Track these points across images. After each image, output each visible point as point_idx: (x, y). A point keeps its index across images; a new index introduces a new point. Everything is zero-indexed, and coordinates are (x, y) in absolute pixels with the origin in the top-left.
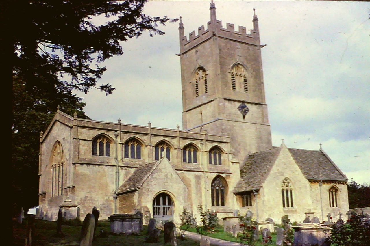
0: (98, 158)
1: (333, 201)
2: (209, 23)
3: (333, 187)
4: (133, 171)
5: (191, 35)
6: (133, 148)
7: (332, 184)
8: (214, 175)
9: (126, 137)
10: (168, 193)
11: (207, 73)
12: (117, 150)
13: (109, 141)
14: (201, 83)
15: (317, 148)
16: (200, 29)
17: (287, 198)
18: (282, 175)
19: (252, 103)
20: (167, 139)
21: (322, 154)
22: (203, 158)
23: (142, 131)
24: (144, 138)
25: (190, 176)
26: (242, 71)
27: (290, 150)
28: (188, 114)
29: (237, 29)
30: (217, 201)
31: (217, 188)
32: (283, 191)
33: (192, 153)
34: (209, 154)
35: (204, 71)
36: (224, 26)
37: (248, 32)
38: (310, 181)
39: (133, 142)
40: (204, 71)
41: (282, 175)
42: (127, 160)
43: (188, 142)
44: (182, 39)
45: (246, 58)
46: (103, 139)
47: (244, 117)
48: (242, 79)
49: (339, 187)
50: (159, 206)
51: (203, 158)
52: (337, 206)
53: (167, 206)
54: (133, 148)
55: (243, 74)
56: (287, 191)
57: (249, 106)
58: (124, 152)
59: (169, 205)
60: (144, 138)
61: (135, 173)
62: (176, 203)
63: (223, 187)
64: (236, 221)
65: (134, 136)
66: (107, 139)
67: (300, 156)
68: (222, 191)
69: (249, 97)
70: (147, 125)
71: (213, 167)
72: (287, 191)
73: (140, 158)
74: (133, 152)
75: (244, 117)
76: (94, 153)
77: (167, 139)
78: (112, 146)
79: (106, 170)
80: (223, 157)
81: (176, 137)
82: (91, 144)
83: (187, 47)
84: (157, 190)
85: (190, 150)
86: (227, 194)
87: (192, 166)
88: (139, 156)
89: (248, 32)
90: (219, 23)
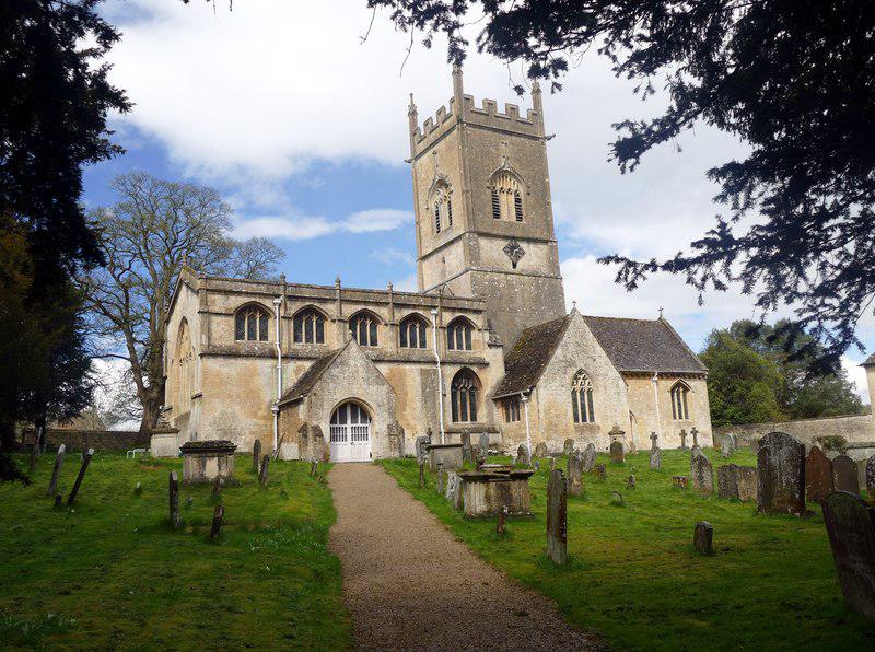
0: (244, 344)
1: (680, 411)
2: (452, 101)
3: (678, 385)
4: (308, 365)
5: (426, 124)
9: (294, 308)
11: (452, 188)
12: (278, 333)
13: (266, 314)
14: (444, 208)
15: (655, 318)
16: (439, 113)
17: (583, 410)
18: (572, 364)
22: (435, 341)
23: (381, 299)
25: (413, 373)
26: (509, 184)
27: (588, 319)
29: (501, 110)
30: (462, 414)
32: (574, 392)
33: (463, 333)
34: (295, 324)
35: (447, 186)
36: (478, 105)
37: (523, 115)
38: (625, 375)
40: (447, 186)
42: (297, 346)
43: (407, 312)
44: (414, 131)
45: (518, 160)
47: (514, 266)
51: (435, 341)
52: (687, 417)
53: (338, 425)
54: (459, 336)
55: (514, 188)
56: (582, 392)
58: (292, 331)
61: (313, 367)
62: (375, 418)
63: (473, 388)
64: (453, 456)
65: (308, 303)
68: (472, 395)
69: (529, 225)
70: (333, 284)
72: (582, 392)
75: (514, 266)
78: (270, 321)
80: (475, 335)
81: (388, 304)
82: (232, 321)
84: (340, 396)
85: (412, 326)
87: (417, 352)
88: (321, 339)
89: (523, 115)
90: (469, 99)
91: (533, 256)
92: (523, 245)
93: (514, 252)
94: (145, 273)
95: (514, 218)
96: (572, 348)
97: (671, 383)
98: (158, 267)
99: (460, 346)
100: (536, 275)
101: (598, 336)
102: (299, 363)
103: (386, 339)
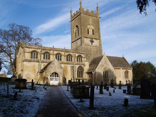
6: (79, 59)
7: (126, 70)
8: (79, 66)
10: (57, 72)
15: (122, 57)
19: (95, 39)
20: (60, 52)
21: (123, 58)
23: (51, 49)
24: (51, 52)
27: (107, 56)
28: (73, 43)
31: (80, 71)
39: (47, 54)
41: (104, 66)
46: (35, 52)
47: (92, 44)
48: (92, 30)
49: (129, 71)
50: (53, 77)
52: (128, 78)
54: (79, 59)
57: (94, 40)
59: (57, 77)
60: (51, 52)
66: (60, 54)
67: (111, 59)
68: (82, 72)
71: (45, 60)
73: (61, 60)
74: (47, 57)
75: (92, 44)
76: (67, 60)
77: (60, 52)
79: (35, 64)
80: (83, 59)
82: (30, 54)
83: (73, 19)
84: (53, 71)
86: (83, 73)
88: (49, 59)
91: (96, 43)
92: (94, 40)
93: (92, 42)
94: (14, 44)
95: (92, 34)
96: (103, 62)
97: (125, 70)
98: (17, 43)
99: (79, 61)
100: (97, 46)
101: (110, 60)
102: (44, 63)
103: (64, 59)
